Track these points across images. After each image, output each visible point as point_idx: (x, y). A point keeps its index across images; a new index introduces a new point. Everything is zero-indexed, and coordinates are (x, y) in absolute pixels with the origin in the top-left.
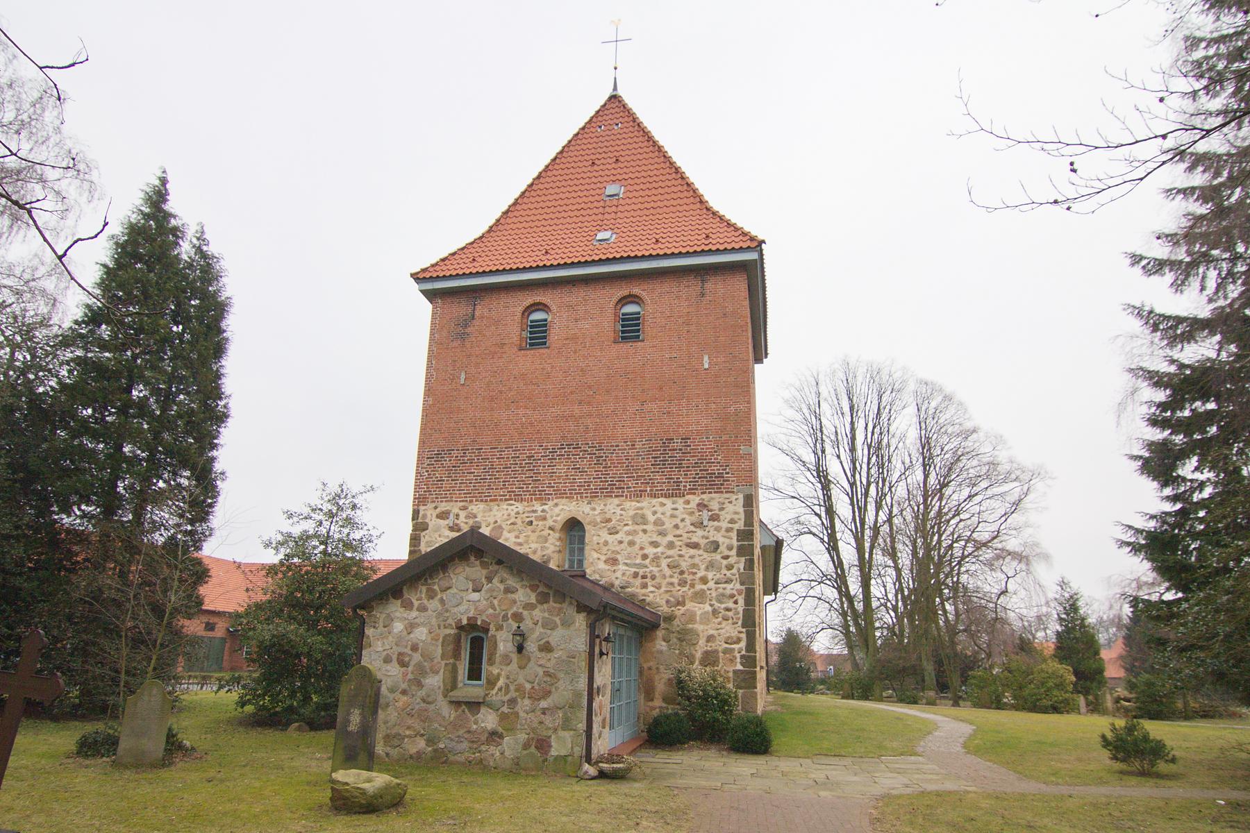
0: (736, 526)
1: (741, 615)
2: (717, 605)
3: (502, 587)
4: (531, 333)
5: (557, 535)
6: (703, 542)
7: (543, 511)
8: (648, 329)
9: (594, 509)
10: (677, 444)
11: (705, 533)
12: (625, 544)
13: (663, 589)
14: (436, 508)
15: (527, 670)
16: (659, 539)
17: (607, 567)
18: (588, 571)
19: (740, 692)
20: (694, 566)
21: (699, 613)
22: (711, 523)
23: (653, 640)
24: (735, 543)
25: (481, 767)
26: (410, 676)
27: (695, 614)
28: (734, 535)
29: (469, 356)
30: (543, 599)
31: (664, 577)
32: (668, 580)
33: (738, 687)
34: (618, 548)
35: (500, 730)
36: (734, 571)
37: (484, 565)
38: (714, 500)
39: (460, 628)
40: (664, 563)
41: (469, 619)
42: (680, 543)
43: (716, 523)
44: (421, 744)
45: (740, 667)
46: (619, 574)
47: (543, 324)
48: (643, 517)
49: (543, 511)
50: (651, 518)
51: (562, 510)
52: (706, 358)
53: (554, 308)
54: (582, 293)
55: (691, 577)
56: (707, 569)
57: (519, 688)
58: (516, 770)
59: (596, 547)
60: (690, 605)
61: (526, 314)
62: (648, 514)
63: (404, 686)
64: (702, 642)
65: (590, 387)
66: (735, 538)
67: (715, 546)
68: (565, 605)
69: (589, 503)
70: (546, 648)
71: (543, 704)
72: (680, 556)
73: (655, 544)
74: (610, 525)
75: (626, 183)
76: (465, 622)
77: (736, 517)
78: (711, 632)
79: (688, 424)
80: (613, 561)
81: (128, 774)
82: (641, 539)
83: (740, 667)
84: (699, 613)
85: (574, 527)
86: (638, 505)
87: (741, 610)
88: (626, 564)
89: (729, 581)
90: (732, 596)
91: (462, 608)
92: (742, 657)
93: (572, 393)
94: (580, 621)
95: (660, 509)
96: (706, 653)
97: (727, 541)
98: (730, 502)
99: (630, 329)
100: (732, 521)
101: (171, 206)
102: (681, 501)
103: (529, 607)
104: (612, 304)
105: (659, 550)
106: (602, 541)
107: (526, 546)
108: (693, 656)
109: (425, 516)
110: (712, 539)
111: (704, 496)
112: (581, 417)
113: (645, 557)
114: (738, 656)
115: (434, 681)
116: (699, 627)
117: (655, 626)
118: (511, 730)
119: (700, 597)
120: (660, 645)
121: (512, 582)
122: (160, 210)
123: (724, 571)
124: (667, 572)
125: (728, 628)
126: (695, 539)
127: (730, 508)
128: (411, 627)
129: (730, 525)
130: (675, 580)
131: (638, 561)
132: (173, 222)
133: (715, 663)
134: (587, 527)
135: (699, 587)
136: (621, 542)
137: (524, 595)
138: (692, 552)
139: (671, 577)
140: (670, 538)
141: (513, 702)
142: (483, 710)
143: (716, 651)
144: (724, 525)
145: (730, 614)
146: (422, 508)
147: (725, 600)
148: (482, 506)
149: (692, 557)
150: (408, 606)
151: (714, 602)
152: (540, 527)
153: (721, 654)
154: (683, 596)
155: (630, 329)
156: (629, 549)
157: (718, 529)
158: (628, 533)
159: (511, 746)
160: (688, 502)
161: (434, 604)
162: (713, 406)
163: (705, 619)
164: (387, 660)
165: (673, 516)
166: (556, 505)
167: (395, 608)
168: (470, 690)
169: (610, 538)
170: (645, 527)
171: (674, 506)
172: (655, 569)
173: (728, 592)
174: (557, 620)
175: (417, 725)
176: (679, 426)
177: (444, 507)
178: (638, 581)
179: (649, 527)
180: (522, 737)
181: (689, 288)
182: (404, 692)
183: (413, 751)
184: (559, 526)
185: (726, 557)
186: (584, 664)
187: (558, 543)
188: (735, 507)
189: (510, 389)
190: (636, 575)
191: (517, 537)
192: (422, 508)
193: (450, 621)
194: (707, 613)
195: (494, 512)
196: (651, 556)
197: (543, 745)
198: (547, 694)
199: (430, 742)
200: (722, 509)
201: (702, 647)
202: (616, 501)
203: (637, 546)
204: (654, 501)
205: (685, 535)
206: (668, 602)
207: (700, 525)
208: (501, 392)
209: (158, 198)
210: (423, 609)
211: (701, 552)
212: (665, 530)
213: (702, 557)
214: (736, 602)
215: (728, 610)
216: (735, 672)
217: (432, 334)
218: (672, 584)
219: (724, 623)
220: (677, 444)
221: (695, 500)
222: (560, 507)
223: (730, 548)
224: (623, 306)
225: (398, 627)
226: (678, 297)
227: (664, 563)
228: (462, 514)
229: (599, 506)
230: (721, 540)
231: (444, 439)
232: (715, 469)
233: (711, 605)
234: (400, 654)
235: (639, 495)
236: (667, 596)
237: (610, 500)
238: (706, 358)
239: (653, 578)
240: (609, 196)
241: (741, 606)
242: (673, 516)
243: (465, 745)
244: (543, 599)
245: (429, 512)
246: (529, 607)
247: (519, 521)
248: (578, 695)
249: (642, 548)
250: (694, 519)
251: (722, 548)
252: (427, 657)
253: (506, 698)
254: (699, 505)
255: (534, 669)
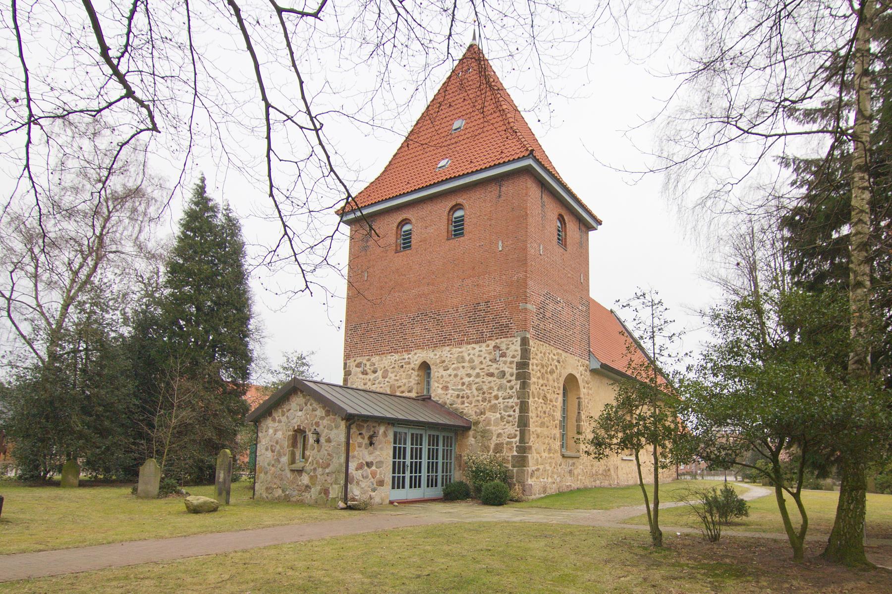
0: (516, 360)
1: (517, 419)
2: (504, 413)
3: (311, 408)
4: (455, 226)
5: (416, 373)
6: (496, 372)
7: (409, 358)
8: (467, 227)
9: (436, 355)
10: (482, 306)
11: (498, 366)
12: (452, 376)
13: (473, 404)
14: (355, 361)
15: (321, 453)
16: (471, 372)
17: (443, 392)
18: (432, 395)
19: (515, 470)
20: (491, 388)
21: (493, 419)
22: (501, 359)
23: (468, 437)
24: (515, 371)
25: (301, 503)
26: (275, 457)
27: (491, 420)
28: (514, 366)
29: (369, 261)
30: (328, 413)
31: (474, 396)
32: (476, 398)
33: (513, 466)
34: (448, 380)
35: (310, 484)
36: (514, 390)
37: (304, 396)
38: (503, 343)
39: (295, 431)
40: (474, 387)
41: (298, 426)
42: (483, 374)
43: (504, 359)
44: (280, 492)
45: (515, 453)
46: (449, 396)
47: (409, 233)
48: (463, 358)
49: (409, 358)
50: (467, 358)
51: (418, 357)
52: (500, 243)
53: (413, 221)
54: (430, 208)
55: (489, 396)
56: (498, 390)
57: (318, 463)
58: (316, 504)
59: (436, 379)
60: (488, 414)
61: (451, 214)
62: (466, 355)
63: (273, 462)
64: (494, 438)
65: (433, 273)
66: (515, 368)
67: (503, 374)
68: (336, 417)
69: (433, 351)
70: (329, 440)
71: (327, 471)
72: (483, 382)
73: (469, 375)
74: (444, 364)
75: (464, 117)
76: (296, 428)
77: (516, 353)
78: (500, 431)
79: (489, 292)
80: (446, 388)
81: (140, 500)
82: (462, 372)
83: (515, 453)
84: (493, 419)
85: (425, 367)
86: (460, 350)
87: (517, 416)
88: (453, 389)
89: (510, 397)
90: (512, 407)
91: (295, 421)
92: (517, 446)
93: (423, 278)
94: (343, 424)
95: (472, 352)
96: (497, 444)
97: (510, 370)
98: (513, 344)
99: (458, 229)
100: (513, 357)
101: (210, 193)
102: (484, 345)
103: (322, 418)
104: (446, 212)
105: (471, 379)
106: (440, 376)
107: (400, 381)
108: (489, 447)
109: (349, 366)
110: (501, 370)
111: (497, 341)
112: (428, 294)
113: (463, 384)
114: (515, 446)
115: (285, 459)
116: (493, 428)
117: (469, 428)
118: (314, 484)
119: (494, 408)
120: (471, 440)
121: (315, 405)
122: (202, 198)
123: (508, 391)
124: (476, 393)
125: (509, 428)
126: (492, 371)
127: (513, 347)
128: (276, 431)
129: (512, 359)
130: (480, 398)
131: (460, 387)
132: (211, 204)
133: (501, 451)
134: (432, 367)
135: (494, 402)
136: (450, 375)
137: (320, 412)
138: (490, 379)
139: (478, 396)
140: (477, 370)
141: (315, 469)
142: (304, 474)
143: (502, 443)
144: (509, 359)
145: (511, 419)
146: (348, 361)
147: (509, 410)
148: (377, 358)
149: (490, 382)
150: (274, 420)
151: (502, 411)
152: (407, 369)
153: (505, 445)
154: (484, 409)
155: (458, 229)
156: (455, 380)
157: (505, 363)
158: (454, 369)
159: (314, 491)
160: (488, 346)
161: (284, 419)
162: (504, 277)
163: (497, 424)
164: (267, 449)
165: (479, 356)
166: (416, 354)
167: (269, 422)
168: (299, 465)
169: (444, 373)
170: (464, 364)
171: (480, 349)
172: (469, 392)
173: (510, 404)
174: (333, 425)
175: (278, 482)
176: (484, 294)
177: (359, 360)
178: (460, 400)
179: (466, 364)
180: (319, 488)
181: (491, 192)
182: (273, 466)
183: (277, 495)
184: (417, 367)
185: (509, 381)
186: (343, 449)
187: (417, 378)
188: (515, 347)
189: (391, 280)
190: (458, 396)
191: (396, 376)
192: (348, 361)
193: (291, 428)
194: (497, 418)
195: (384, 361)
196: (467, 383)
197: (326, 492)
198: (328, 465)
199: (283, 491)
200: (507, 349)
201: (494, 440)
202: (448, 348)
203: (459, 377)
204: (469, 346)
205: (486, 368)
206: (476, 412)
207: (494, 361)
208: (386, 282)
209: (201, 190)
210: (280, 422)
211: (495, 379)
212: (475, 365)
213: (495, 381)
214: (514, 411)
215: (510, 416)
216: (513, 456)
217: (350, 249)
218: (478, 401)
219: (508, 425)
220: (482, 306)
221: (492, 343)
222: (418, 355)
223: (512, 375)
224: (454, 213)
225: (271, 431)
226: (485, 201)
227: (474, 387)
228: (368, 364)
229: (438, 352)
230: (506, 369)
231: (358, 317)
232: (504, 321)
233: (500, 414)
234: (272, 446)
235: (460, 343)
236: (475, 409)
237: (444, 348)
238: (500, 243)
239: (468, 397)
240: (455, 130)
241: (517, 414)
242: (479, 356)
243: (296, 493)
244: (328, 413)
245: (352, 364)
246: (322, 418)
247: (396, 366)
248: (341, 465)
249: (462, 379)
250: (492, 357)
251: (507, 375)
252: (282, 447)
253: (312, 468)
254: (494, 347)
255: (324, 452)
